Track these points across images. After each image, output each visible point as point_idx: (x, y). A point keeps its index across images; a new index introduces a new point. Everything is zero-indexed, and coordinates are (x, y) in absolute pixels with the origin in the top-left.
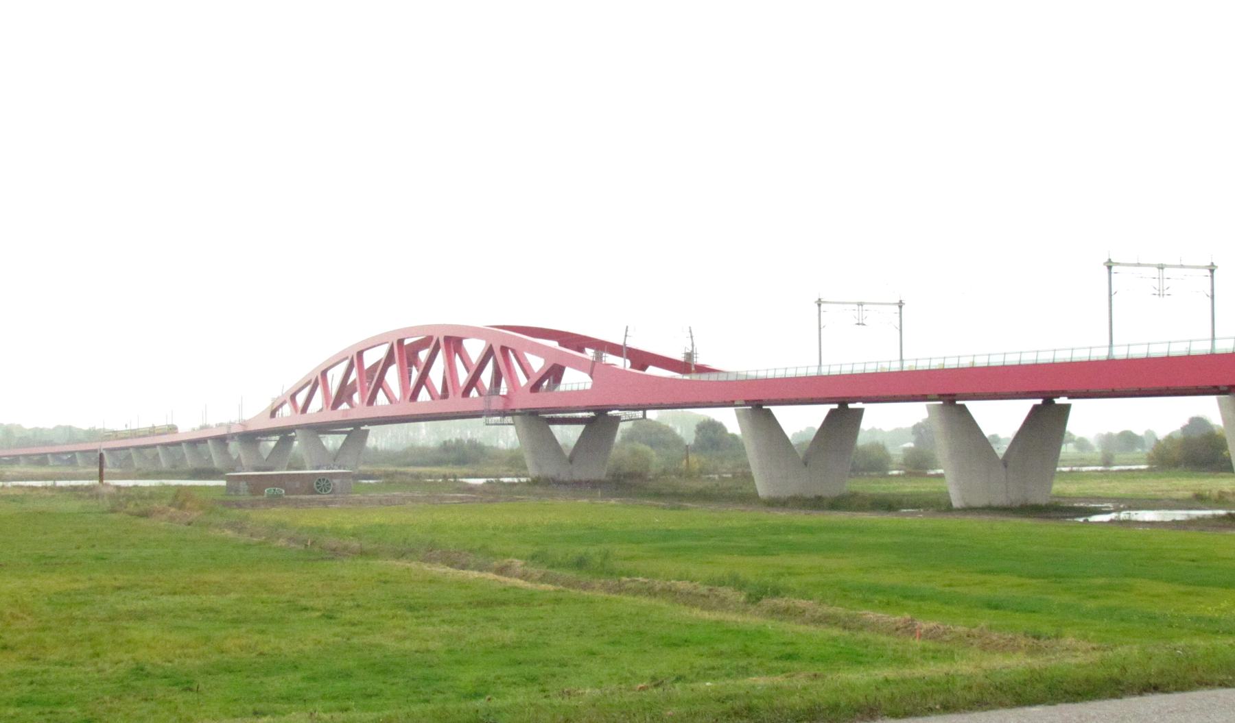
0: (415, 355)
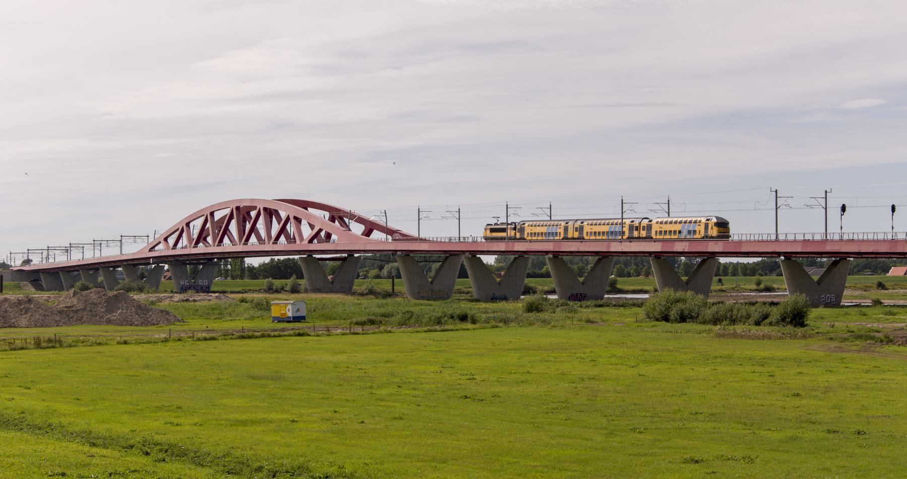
0: (248, 213)
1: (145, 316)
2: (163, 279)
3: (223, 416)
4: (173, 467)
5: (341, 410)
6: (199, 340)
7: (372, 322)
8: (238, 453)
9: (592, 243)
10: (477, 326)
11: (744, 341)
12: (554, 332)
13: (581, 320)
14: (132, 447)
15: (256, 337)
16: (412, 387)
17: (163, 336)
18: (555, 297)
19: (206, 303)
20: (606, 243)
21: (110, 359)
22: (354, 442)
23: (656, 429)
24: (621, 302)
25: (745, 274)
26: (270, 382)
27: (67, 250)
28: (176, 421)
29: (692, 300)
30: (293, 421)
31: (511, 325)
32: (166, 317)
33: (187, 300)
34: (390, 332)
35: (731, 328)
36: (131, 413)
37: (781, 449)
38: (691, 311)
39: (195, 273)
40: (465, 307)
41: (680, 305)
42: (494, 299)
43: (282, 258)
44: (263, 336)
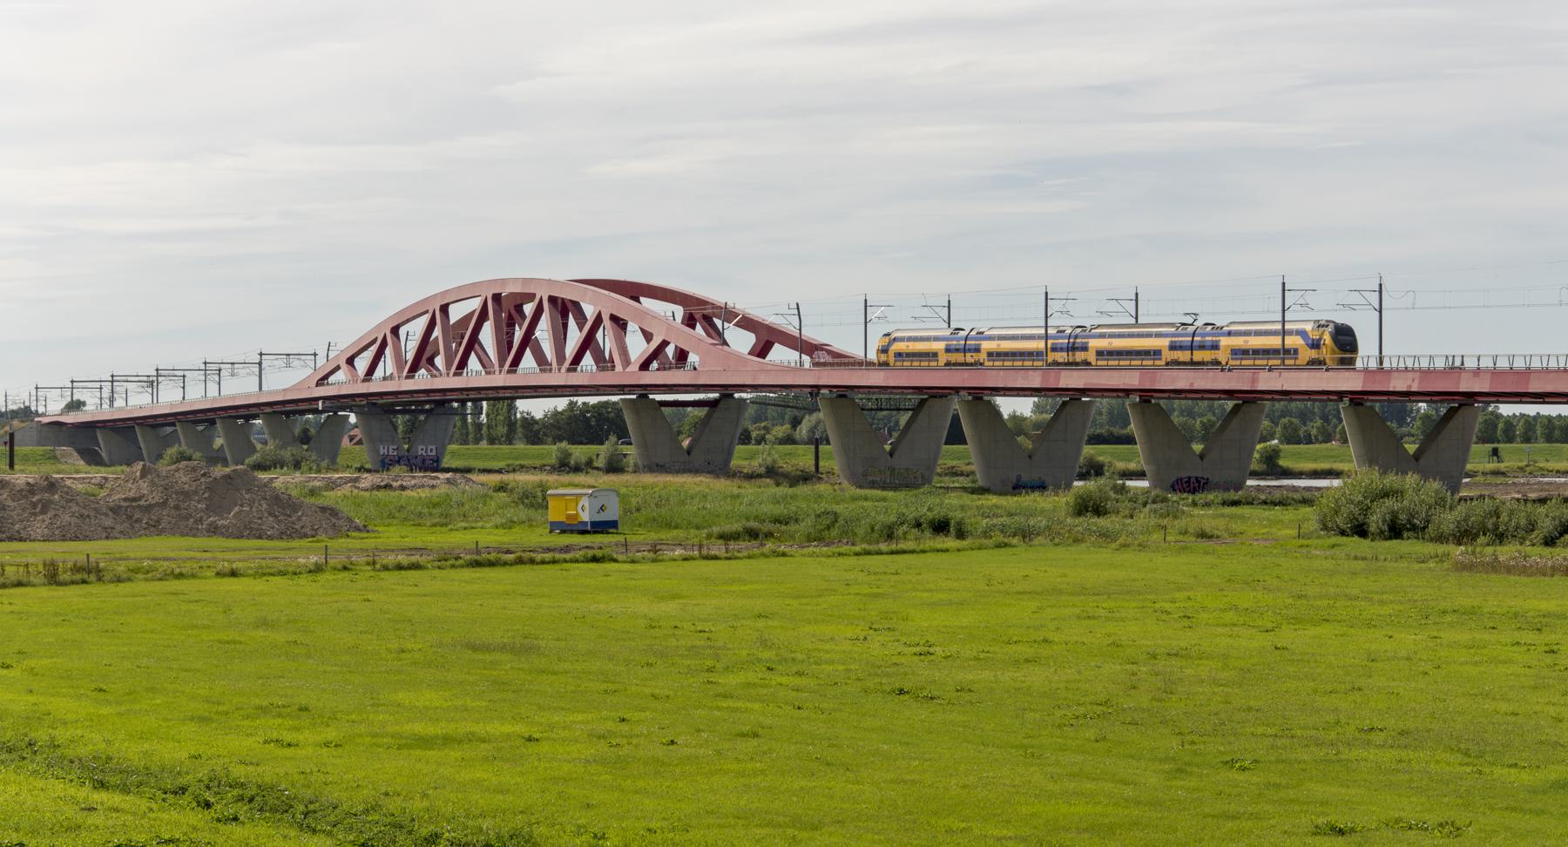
1: (288, 520)
2: (345, 442)
3: (390, 729)
4: (255, 830)
5: (637, 716)
6: (386, 568)
7: (753, 534)
8: (393, 805)
9: (1116, 374)
10: (964, 543)
11: (1512, 578)
12: (1127, 556)
13: (1186, 533)
14: (183, 790)
15: (505, 564)
16: (795, 669)
17: (313, 559)
18: (1145, 484)
19: (424, 493)
20: (1248, 374)
21: (192, 607)
22: (641, 784)
23: (1278, 761)
24: (1277, 495)
25: (1549, 439)
26: (505, 657)
27: (152, 383)
28: (288, 737)
29: (1416, 490)
30: (530, 739)
31: (1036, 542)
32: (334, 520)
33: (388, 487)
34: (784, 555)
35: (1490, 550)
36: (203, 720)
37: (1527, 806)
38: (1412, 516)
39: (412, 428)
40: (953, 504)
41: (1389, 503)
42: (1018, 488)
43: (593, 400)
44: (520, 561)
